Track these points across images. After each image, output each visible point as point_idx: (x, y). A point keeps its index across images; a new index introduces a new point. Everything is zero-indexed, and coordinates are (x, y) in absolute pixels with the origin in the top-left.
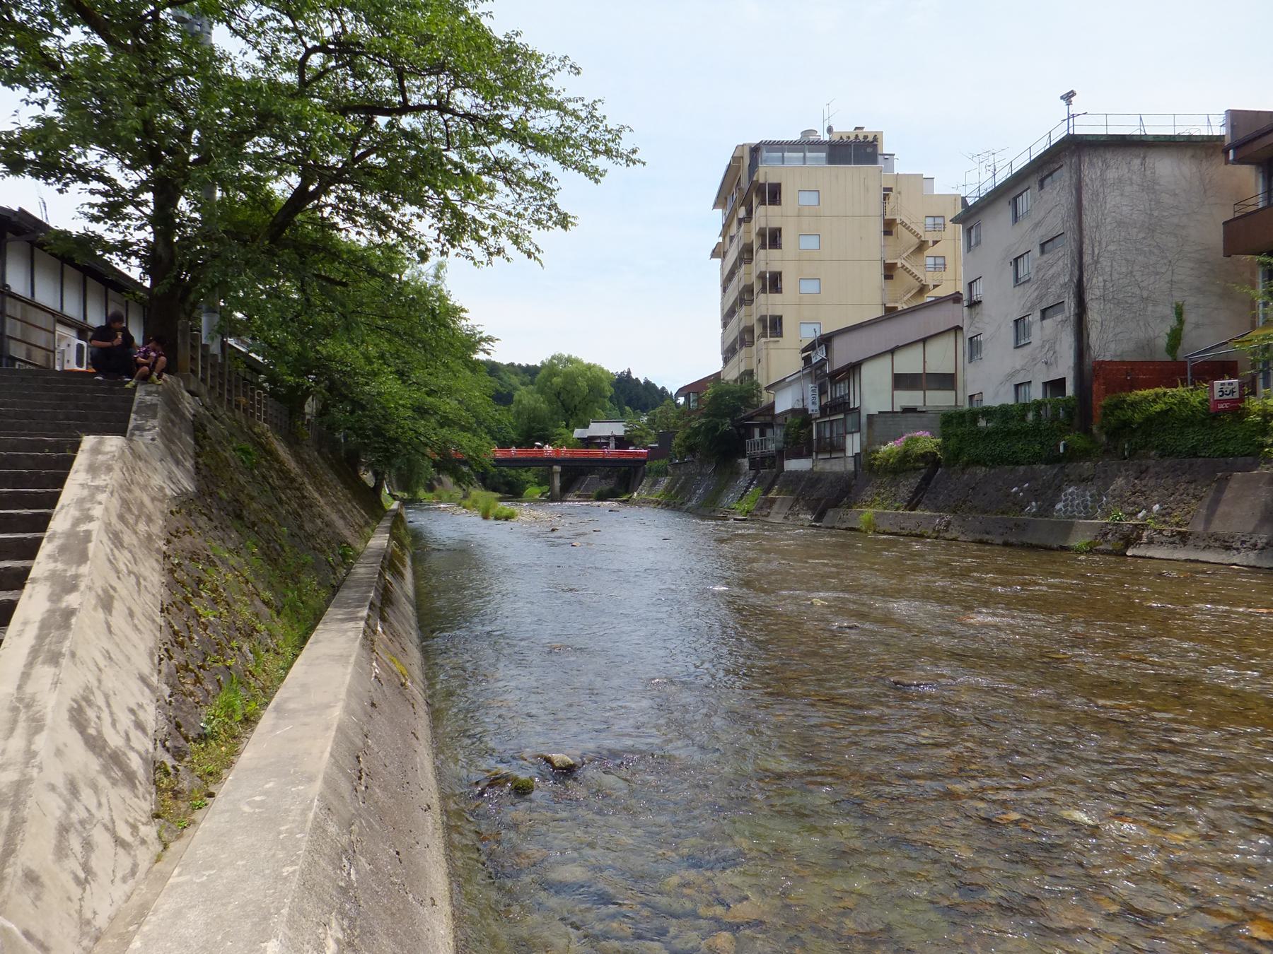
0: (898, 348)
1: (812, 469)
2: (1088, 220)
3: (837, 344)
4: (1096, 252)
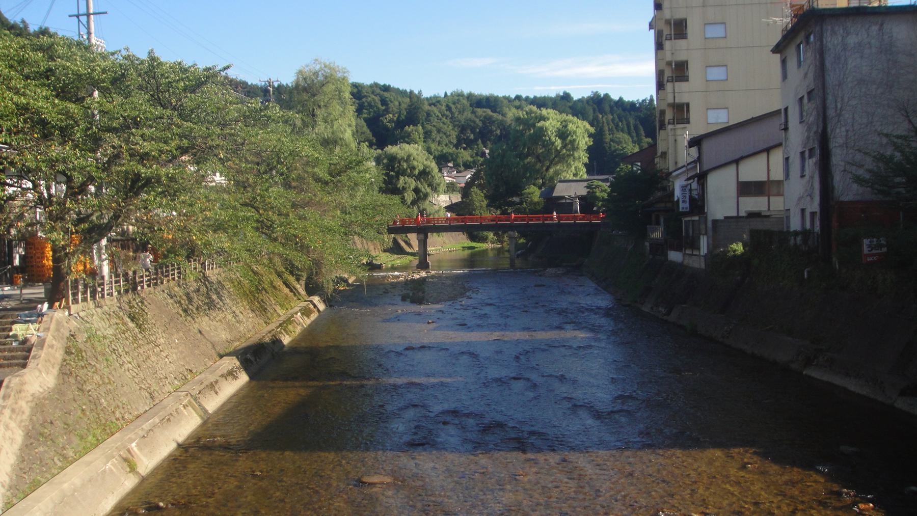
0: (743, 158)
1: (682, 262)
2: (832, 79)
3: (706, 145)
4: (839, 105)
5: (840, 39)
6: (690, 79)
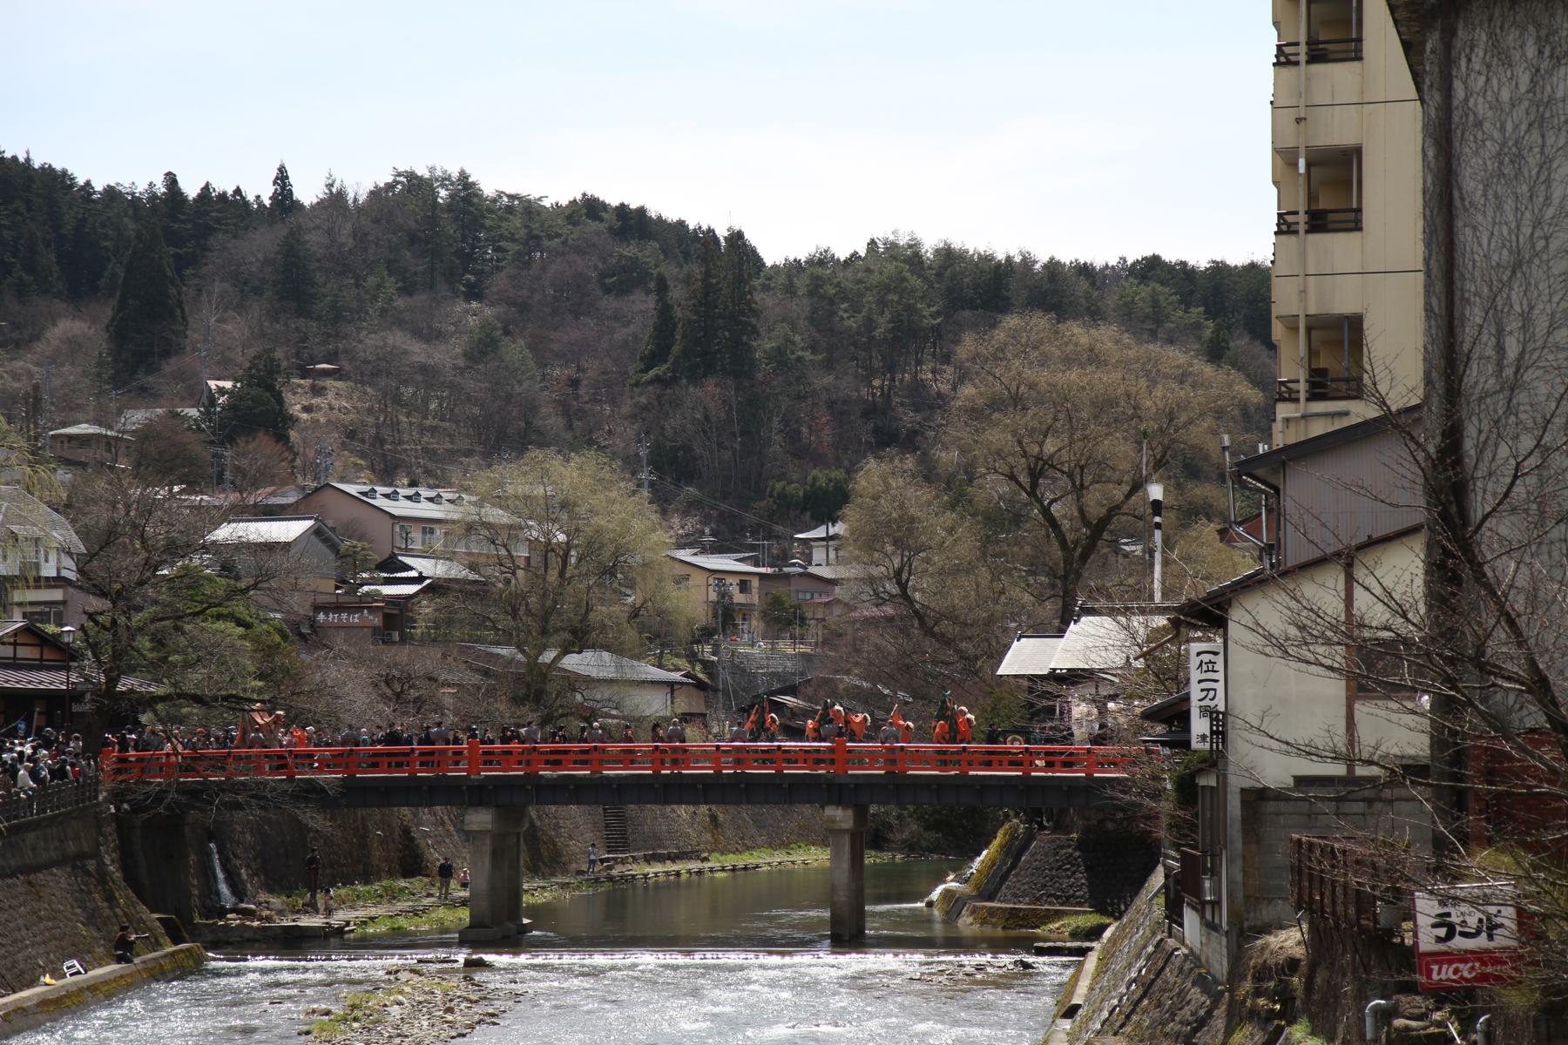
4: (1512, 348)
5: (1525, 79)
6: (1366, 223)
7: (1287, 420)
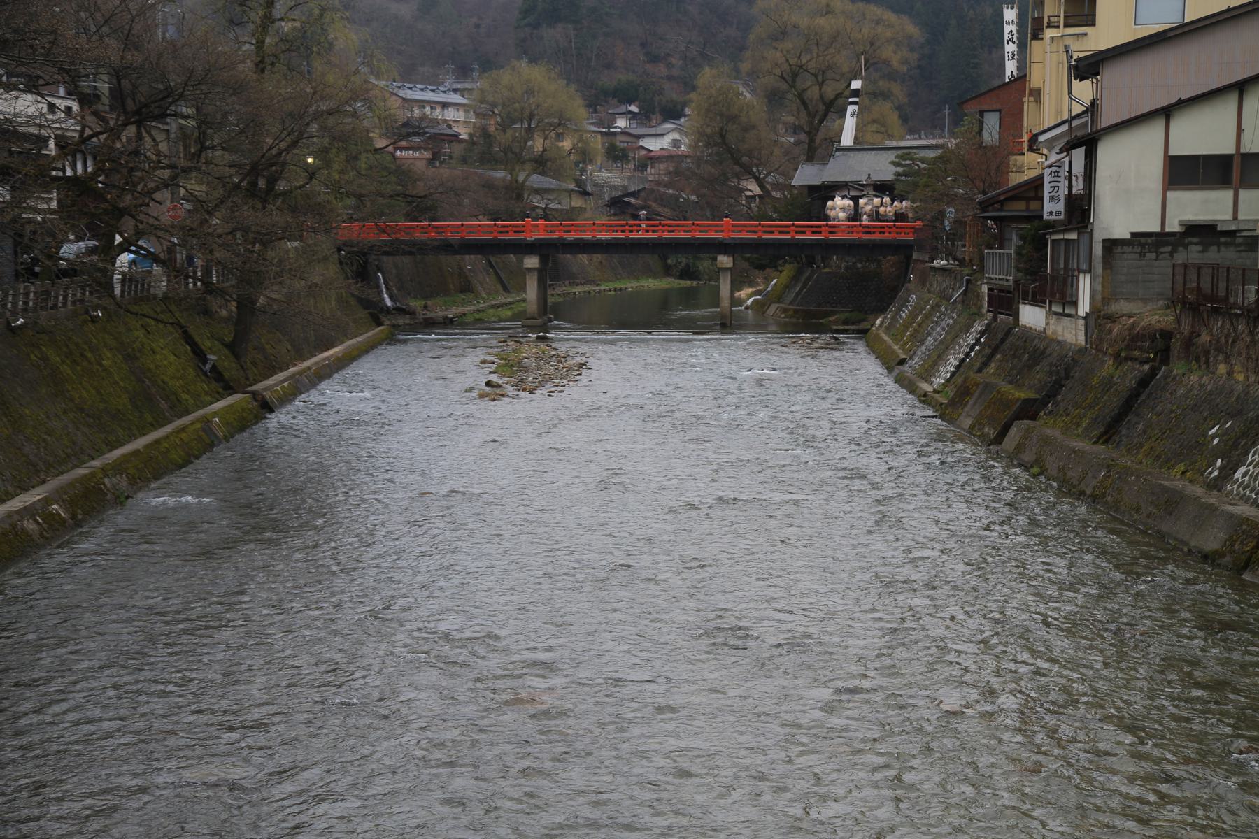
7: (1052, 38)
